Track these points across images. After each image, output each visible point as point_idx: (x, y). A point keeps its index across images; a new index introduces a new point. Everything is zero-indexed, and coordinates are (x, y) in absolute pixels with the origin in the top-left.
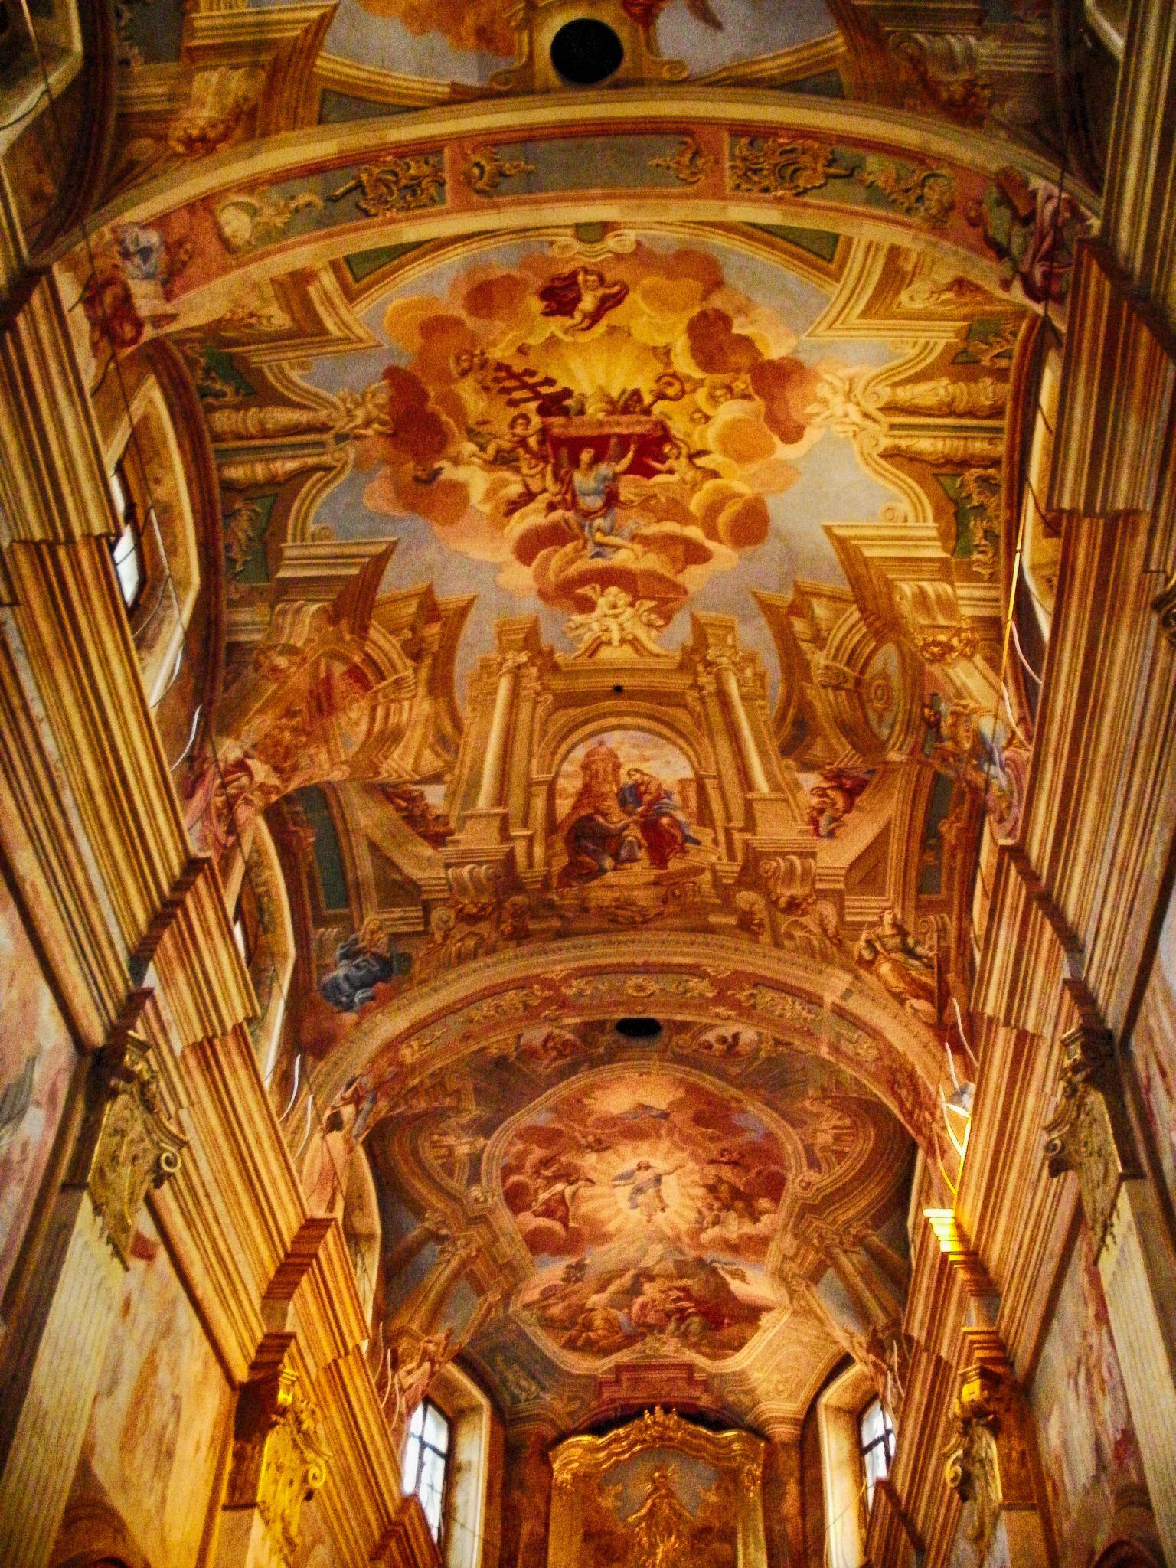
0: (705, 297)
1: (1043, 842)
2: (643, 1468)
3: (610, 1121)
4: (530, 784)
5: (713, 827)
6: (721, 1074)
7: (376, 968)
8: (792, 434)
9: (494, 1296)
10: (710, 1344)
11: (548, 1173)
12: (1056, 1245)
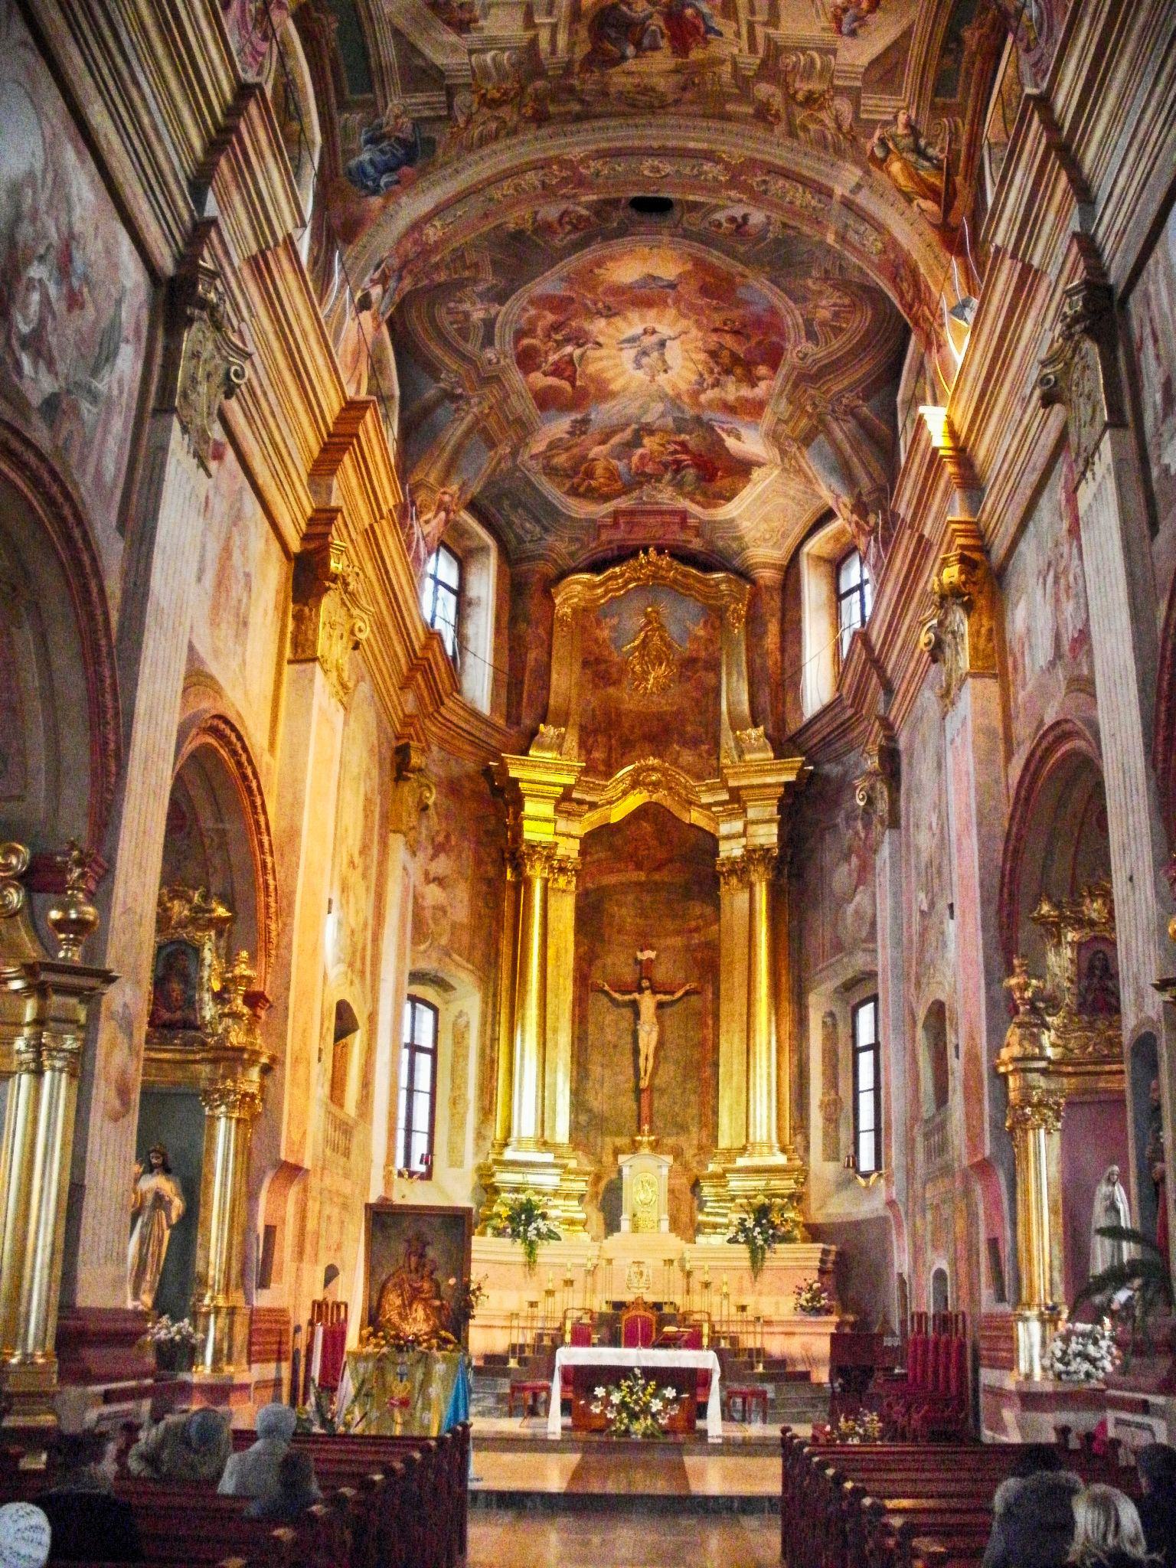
1: (1070, 95)
2: (637, 603)
3: (618, 291)
6: (730, 253)
7: (400, 152)
9: (505, 449)
10: (705, 494)
11: (559, 337)
12: (1040, 458)
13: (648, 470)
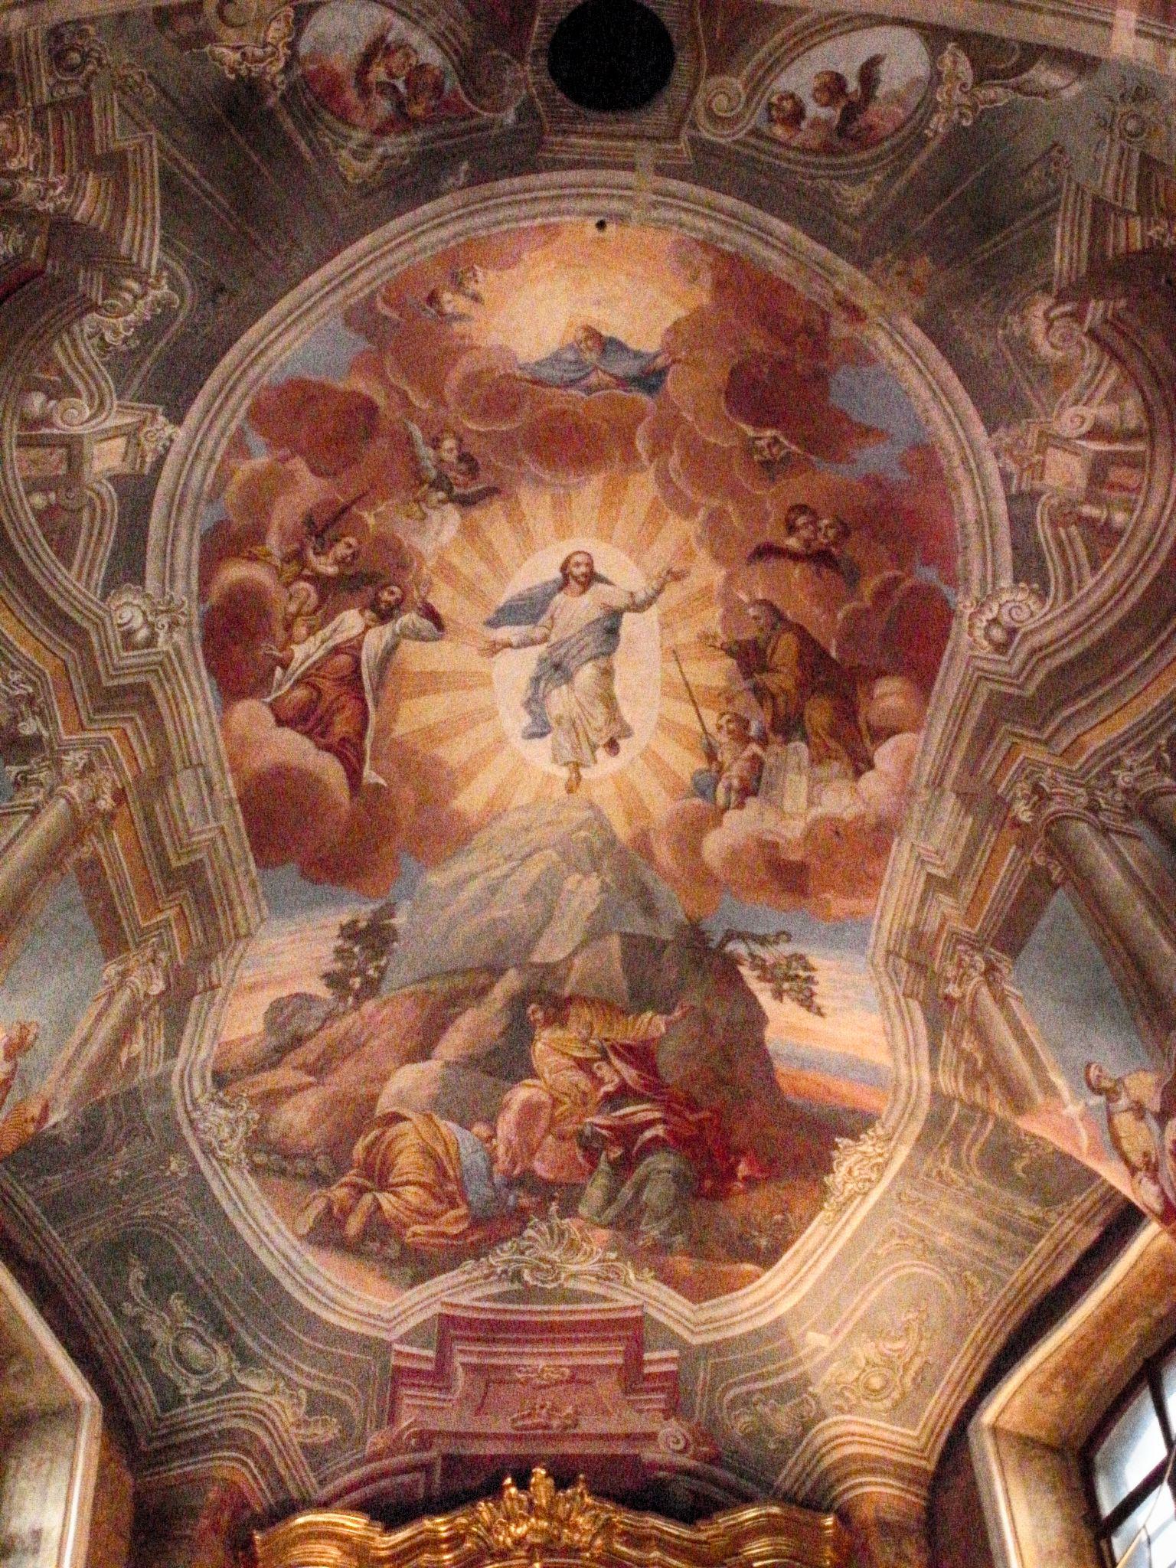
10: (697, 1249)
13: (541, 1168)
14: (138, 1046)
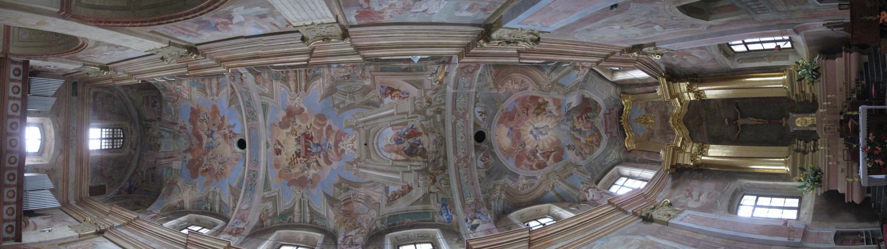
0: (277, 126)
3: (514, 143)
4: (392, 165)
5: (407, 122)
8: (302, 109)
13: (590, 126)
14: (582, 170)
